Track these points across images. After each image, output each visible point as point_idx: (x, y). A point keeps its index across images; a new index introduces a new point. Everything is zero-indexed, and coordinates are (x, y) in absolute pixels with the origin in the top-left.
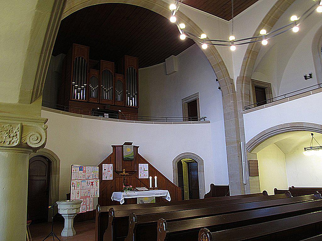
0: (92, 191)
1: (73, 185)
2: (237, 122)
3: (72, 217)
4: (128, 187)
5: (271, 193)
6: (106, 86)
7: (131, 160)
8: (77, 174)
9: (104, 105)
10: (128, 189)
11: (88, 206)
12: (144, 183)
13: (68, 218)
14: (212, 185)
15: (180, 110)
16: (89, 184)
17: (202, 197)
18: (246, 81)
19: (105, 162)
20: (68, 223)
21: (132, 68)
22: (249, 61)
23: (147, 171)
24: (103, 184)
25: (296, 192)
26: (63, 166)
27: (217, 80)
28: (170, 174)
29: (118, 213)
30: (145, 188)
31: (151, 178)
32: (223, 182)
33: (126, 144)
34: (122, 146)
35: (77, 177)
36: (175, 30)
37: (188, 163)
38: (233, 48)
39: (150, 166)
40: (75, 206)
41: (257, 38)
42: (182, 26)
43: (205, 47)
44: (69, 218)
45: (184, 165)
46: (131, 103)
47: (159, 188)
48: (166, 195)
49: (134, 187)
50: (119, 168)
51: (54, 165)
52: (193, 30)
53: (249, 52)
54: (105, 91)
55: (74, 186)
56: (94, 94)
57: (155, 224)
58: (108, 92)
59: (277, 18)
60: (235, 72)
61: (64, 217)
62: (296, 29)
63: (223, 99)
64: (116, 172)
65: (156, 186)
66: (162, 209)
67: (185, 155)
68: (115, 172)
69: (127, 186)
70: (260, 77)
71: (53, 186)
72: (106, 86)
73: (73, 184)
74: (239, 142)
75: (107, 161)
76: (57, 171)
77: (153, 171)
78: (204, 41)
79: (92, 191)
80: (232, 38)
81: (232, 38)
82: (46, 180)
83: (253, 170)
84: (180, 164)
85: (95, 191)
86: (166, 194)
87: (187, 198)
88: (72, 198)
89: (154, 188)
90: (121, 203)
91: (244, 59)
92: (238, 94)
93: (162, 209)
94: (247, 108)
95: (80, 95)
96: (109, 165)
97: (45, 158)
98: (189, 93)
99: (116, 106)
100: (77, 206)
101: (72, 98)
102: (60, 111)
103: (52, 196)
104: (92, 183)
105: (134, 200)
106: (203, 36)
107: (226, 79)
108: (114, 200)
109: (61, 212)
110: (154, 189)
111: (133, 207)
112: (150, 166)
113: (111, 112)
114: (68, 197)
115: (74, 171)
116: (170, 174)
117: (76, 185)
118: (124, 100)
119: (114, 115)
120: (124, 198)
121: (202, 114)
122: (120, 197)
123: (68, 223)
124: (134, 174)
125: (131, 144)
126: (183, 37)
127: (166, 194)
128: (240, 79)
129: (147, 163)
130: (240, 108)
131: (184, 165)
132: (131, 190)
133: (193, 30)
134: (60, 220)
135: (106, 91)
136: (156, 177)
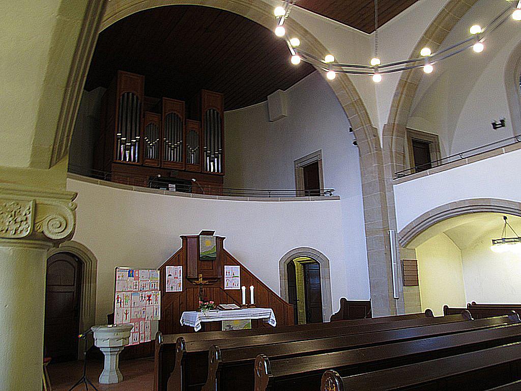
0: (149, 310)
1: (118, 300)
2: (383, 198)
3: (117, 353)
4: (208, 303)
5: (438, 313)
6: (171, 140)
7: (212, 260)
8: (124, 282)
9: (169, 171)
10: (208, 307)
11: (142, 335)
12: (234, 297)
13: (110, 353)
14: (343, 301)
15: (291, 179)
16: (143, 298)
17: (327, 319)
18: (398, 131)
19: (170, 263)
20: (110, 362)
21: (214, 110)
22: (403, 99)
23: (238, 277)
24: (167, 298)
25: (479, 312)
26: (102, 269)
27: (351, 130)
28: (275, 283)
29: (192, 346)
30: (234, 306)
31: (244, 288)
32: (361, 295)
33: (204, 233)
34: (198, 237)
35: (124, 287)
36: (283, 49)
37: (304, 265)
38: (377, 78)
39: (243, 269)
40: (121, 335)
41: (415, 62)
42: (294, 42)
43: (331, 76)
44: (112, 353)
45: (298, 268)
46: (213, 167)
47: (256, 305)
48: (268, 316)
49: (217, 304)
50: (193, 273)
51: (87, 268)
52: (312, 49)
53: (403, 84)
54: (170, 148)
55: (120, 301)
56: (151, 153)
57: (251, 364)
58: (175, 149)
59: (448, 29)
60: (381, 117)
61: (104, 352)
62: (478, 48)
63: (361, 160)
64: (188, 279)
65: (252, 302)
66: (262, 339)
67: (299, 252)
68: (187, 279)
69: (206, 302)
70: (420, 126)
71: (85, 302)
72: (171, 140)
73: (118, 298)
74: (386, 230)
75: (173, 262)
76: (93, 277)
77: (247, 277)
78: (330, 66)
79: (149, 310)
80: (375, 62)
81: (375, 62)
82: (74, 292)
83: (410, 276)
84: (291, 266)
85: (154, 310)
86: (268, 314)
87: (303, 321)
88: (117, 320)
89: (249, 305)
90: (196, 330)
91: (395, 95)
92: (385, 153)
93: (262, 339)
94: (400, 176)
95: (129, 154)
96: (176, 267)
97: (73, 256)
98: (306, 152)
99: (187, 171)
100: (125, 334)
101: (116, 159)
102: (97, 180)
103: (85, 318)
104: (149, 297)
105: (217, 325)
106: (329, 59)
107: (365, 129)
108: (184, 325)
109: (98, 344)
110: (248, 307)
111: (215, 336)
112: (243, 269)
113: (179, 182)
114: (111, 319)
115: (120, 278)
116: (275, 283)
117: (122, 301)
118: (201, 162)
119: (184, 187)
120: (200, 321)
121: (326, 185)
122: (194, 319)
123: (110, 362)
124: (216, 282)
125: (211, 233)
126: (296, 60)
127: (268, 314)
128: (389, 129)
129: (238, 264)
130: (388, 176)
131: (298, 268)
132: (212, 308)
133: (312, 49)
134: (97, 357)
135: (171, 147)
136: (252, 288)
